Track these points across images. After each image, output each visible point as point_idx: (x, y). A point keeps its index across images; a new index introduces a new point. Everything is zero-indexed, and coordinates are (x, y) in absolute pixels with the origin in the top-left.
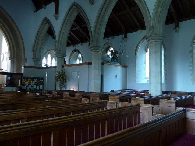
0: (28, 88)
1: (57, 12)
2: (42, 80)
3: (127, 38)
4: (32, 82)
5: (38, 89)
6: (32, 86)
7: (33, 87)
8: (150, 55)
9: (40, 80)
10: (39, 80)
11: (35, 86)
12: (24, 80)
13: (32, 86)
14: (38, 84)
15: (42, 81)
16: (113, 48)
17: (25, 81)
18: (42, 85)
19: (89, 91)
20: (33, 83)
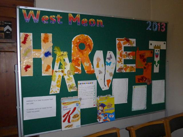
0: (69, 105)
1: (67, 127)
2: (163, 45)
3: (111, 94)
4: (99, 54)
5: (154, 82)
6: (100, 92)
7: (109, 92)
8: (15, 73)
9: (153, 44)
10: (142, 45)
11: (120, 86)
12: (37, 46)
13: (105, 88)
14: (139, 71)
15: (163, 53)
16: (156, 73)
17: (47, 46)
18: (161, 76)
19: (169, 115)
20: (111, 69)
